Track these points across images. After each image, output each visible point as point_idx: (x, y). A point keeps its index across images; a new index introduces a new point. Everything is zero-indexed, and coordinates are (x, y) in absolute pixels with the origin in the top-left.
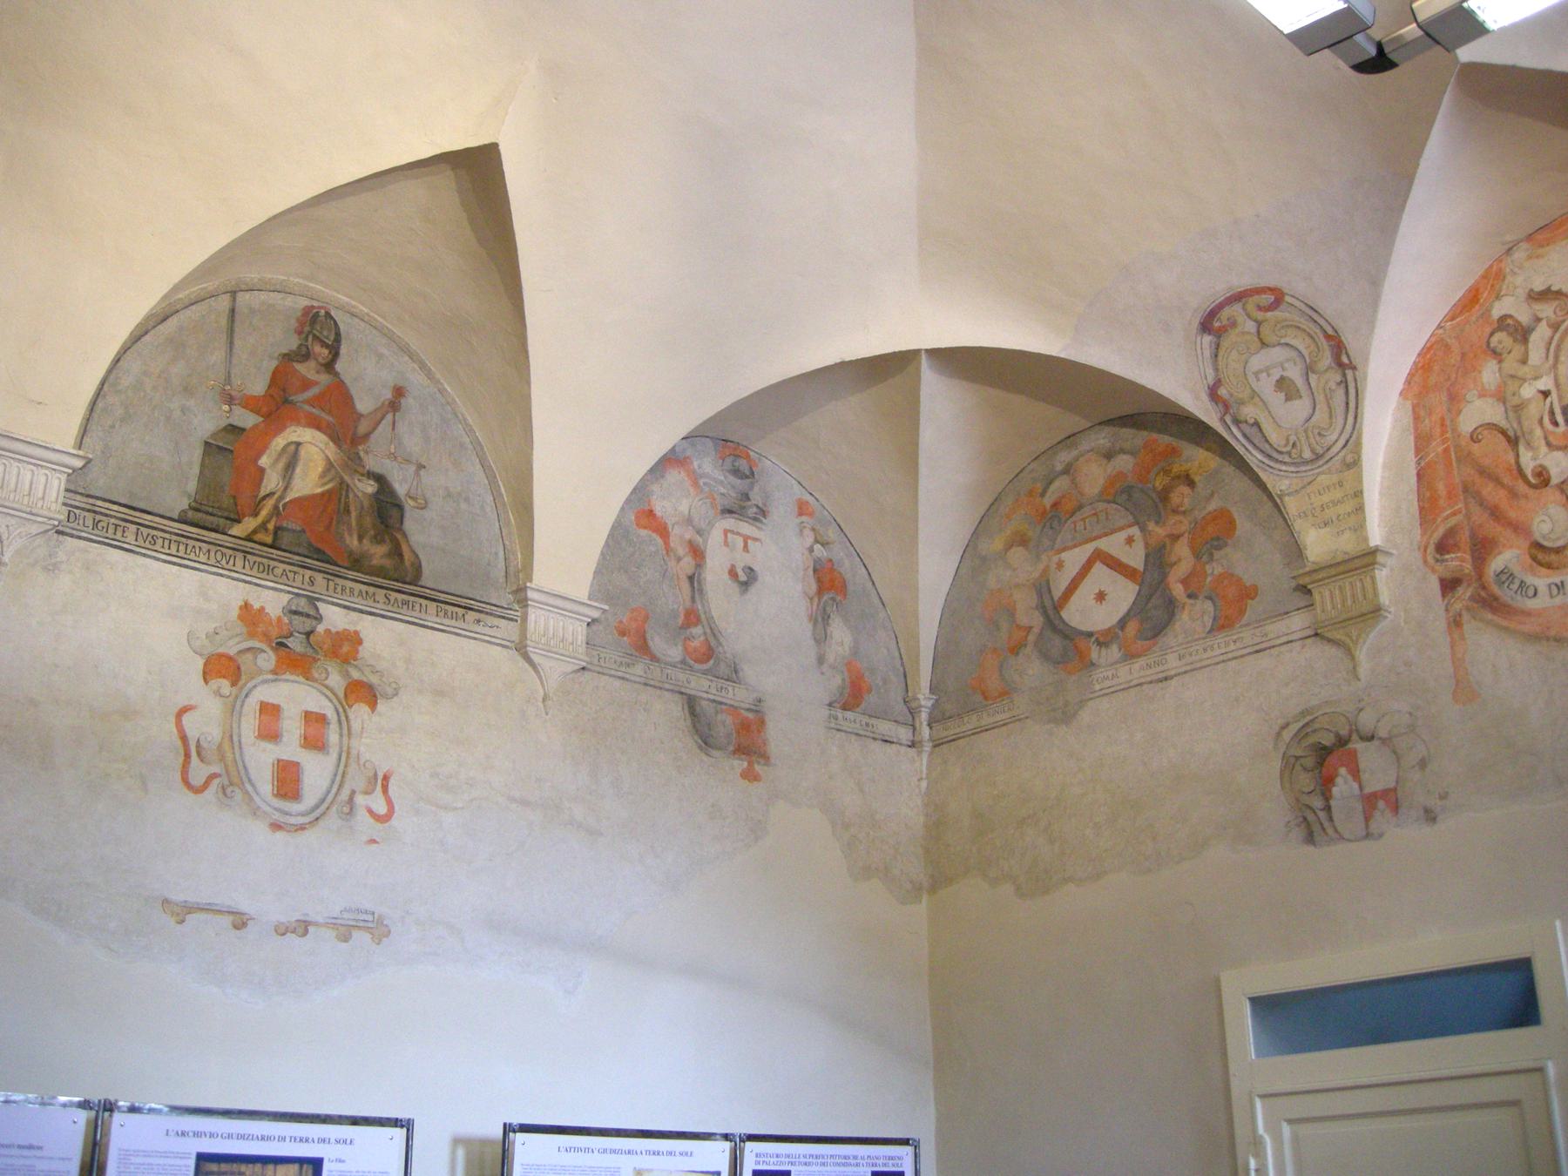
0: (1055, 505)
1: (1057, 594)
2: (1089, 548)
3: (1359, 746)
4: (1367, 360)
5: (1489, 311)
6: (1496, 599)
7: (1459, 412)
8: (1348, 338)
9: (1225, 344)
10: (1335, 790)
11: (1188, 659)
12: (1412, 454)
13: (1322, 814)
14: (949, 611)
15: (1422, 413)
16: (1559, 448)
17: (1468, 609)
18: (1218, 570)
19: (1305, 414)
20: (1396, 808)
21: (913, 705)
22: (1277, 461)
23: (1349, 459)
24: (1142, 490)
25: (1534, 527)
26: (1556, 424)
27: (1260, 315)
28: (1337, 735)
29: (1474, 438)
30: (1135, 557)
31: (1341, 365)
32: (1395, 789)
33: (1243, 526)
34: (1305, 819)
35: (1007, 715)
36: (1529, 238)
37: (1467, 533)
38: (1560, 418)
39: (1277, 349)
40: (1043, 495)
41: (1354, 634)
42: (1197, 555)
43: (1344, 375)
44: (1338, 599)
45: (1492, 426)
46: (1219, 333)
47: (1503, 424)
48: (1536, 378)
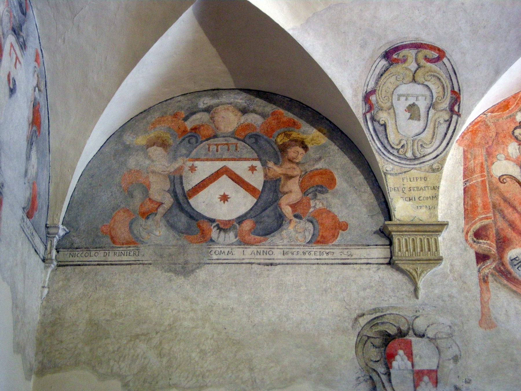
0: (194, 129)
1: (188, 187)
2: (219, 165)
3: (414, 339)
6: (510, 273)
7: (493, 163)
8: (464, 98)
9: (392, 70)
10: (395, 364)
11: (290, 255)
12: (461, 177)
13: (384, 378)
14: (374, 155)
15: (469, 156)
17: (492, 275)
18: (319, 206)
19: (417, 131)
20: (436, 383)
21: (51, 231)
22: (389, 152)
23: (435, 166)
24: (266, 140)
27: (423, 62)
28: (399, 329)
29: (501, 179)
30: (257, 180)
31: (452, 110)
32: (436, 371)
33: (341, 184)
34: (371, 377)
35: (133, 258)
37: (494, 231)
40: (186, 119)
42: (305, 191)
43: (451, 117)
44: (411, 246)
45: (512, 177)
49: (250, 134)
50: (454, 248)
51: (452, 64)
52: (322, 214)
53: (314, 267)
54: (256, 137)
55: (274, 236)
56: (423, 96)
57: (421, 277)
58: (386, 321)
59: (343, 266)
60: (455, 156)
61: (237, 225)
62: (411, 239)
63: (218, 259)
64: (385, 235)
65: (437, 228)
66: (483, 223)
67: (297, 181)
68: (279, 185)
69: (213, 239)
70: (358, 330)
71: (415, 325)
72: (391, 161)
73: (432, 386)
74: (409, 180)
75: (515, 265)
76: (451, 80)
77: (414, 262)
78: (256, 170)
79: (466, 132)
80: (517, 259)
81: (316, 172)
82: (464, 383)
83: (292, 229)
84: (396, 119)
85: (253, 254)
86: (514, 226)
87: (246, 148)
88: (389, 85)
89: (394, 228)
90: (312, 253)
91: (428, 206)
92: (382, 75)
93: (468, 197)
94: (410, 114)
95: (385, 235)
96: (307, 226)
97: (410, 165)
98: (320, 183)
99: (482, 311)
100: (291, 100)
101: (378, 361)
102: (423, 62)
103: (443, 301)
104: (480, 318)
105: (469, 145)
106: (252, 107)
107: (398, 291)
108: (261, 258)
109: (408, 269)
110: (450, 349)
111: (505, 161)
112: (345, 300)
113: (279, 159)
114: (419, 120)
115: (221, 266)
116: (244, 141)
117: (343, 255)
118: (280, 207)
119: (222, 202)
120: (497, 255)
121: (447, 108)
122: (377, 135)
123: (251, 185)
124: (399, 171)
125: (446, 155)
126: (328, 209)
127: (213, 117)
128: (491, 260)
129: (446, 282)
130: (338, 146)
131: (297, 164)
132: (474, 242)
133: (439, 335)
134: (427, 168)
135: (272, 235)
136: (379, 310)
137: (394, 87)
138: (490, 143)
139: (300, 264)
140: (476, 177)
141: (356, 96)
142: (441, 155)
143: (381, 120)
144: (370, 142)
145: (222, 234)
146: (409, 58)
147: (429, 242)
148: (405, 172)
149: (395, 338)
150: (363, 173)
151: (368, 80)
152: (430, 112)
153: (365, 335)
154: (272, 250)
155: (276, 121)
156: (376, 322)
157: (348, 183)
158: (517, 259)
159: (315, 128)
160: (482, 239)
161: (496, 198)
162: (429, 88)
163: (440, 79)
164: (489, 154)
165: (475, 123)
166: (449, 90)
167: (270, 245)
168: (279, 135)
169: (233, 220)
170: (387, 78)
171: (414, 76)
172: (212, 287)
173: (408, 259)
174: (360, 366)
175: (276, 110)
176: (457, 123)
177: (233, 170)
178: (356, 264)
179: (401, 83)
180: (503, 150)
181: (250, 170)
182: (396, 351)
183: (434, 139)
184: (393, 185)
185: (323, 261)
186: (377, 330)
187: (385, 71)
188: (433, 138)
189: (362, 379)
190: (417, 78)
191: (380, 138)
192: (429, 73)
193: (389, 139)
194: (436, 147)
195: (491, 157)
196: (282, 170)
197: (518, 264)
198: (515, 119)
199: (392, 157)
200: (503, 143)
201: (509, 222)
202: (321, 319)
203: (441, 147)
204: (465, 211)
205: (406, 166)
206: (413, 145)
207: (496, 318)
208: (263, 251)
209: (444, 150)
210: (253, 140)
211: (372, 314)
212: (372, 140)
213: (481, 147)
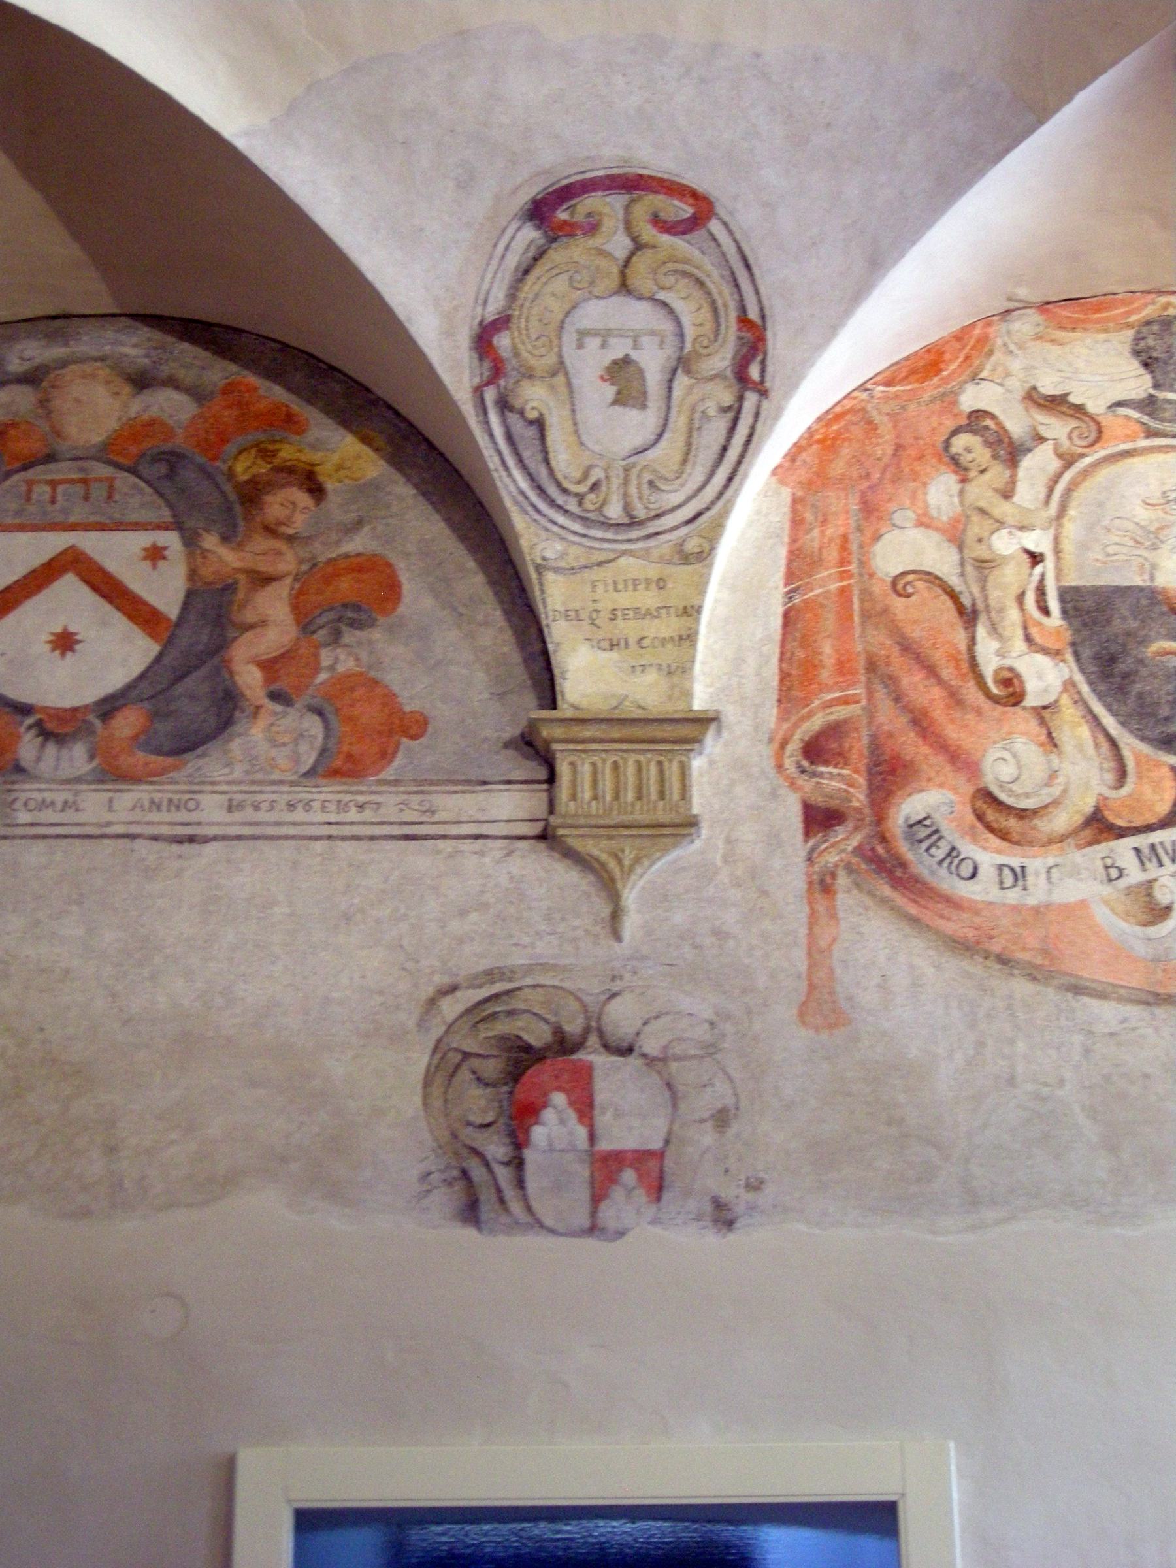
2: (54, 543)
4: (793, 386)
5: (955, 394)
6: (903, 865)
7: (877, 537)
8: (778, 340)
9: (557, 255)
10: (539, 1133)
11: (249, 814)
13: (503, 1174)
15: (809, 516)
16: (1045, 651)
17: (849, 868)
18: (346, 664)
19: (638, 441)
20: (658, 1189)
22: (552, 503)
23: (691, 546)
24: (203, 470)
26: (1046, 611)
27: (648, 233)
28: (558, 1032)
29: (899, 585)
30: (165, 590)
31: (742, 377)
32: (660, 1155)
33: (415, 598)
34: (465, 1174)
36: (1045, 307)
37: (865, 741)
38: (1054, 605)
39: (644, 307)
41: (628, 857)
42: (305, 622)
43: (741, 398)
44: (607, 784)
47: (954, 581)
48: (1022, 528)
49: (155, 451)
50: (739, 790)
51: (738, 236)
52: (352, 689)
53: (319, 846)
54: (174, 459)
55: (204, 755)
56: (653, 333)
57: (633, 877)
58: (522, 1006)
59: (402, 843)
60: (767, 515)
61: (98, 723)
62: (609, 763)
63: (32, 825)
64: (534, 749)
65: (684, 731)
66: (832, 718)
67: (285, 592)
68: (231, 603)
69: (23, 764)
70: (437, 1031)
71: (605, 1020)
74: (611, 588)
75: (920, 841)
76: (737, 286)
77: (613, 832)
78: (164, 558)
79: (804, 442)
80: (927, 822)
81: (342, 564)
82: (742, 1191)
83: (260, 736)
84: (573, 404)
85: (138, 810)
86: (925, 724)
87: (141, 492)
88: (550, 301)
89: (558, 732)
90: (316, 805)
91: (665, 666)
92: (526, 272)
93: (795, 640)
94: (614, 389)
95: (537, 752)
96: (306, 724)
98: (355, 596)
99: (810, 979)
100: (285, 347)
101: (489, 1125)
102: (648, 233)
103: (696, 947)
105: (810, 483)
106: (165, 370)
107: (563, 919)
108: (163, 821)
109: (596, 852)
110: (709, 1089)
111: (915, 531)
112: (405, 942)
113: (235, 526)
114: (644, 406)
115: (41, 845)
116: (133, 471)
117: (407, 811)
118: (228, 667)
119: (57, 653)
120: (867, 811)
121: (729, 373)
123: (145, 604)
124: (583, 562)
125: (725, 513)
126: (373, 674)
127: (48, 400)
128: (850, 825)
129: (711, 891)
130: (416, 486)
131: (290, 539)
132: (803, 772)
133: (678, 1049)
134: (666, 550)
135: (199, 751)
136: (503, 974)
137: (567, 307)
138: (876, 476)
139: (279, 838)
140: (822, 579)
141: (449, 334)
143: (528, 407)
144: (495, 475)
145: (51, 750)
146: (606, 219)
147: (661, 772)
148: (600, 564)
150: (483, 565)
151: (485, 286)
152: (676, 384)
153: (456, 1050)
154: (198, 797)
155: (235, 412)
156: (490, 1008)
157: (436, 597)
158: (927, 822)
159: (351, 431)
160: (826, 763)
164: (869, 509)
165: (831, 417)
166: (733, 315)
167: (191, 783)
168: (240, 452)
169: (86, 707)
170: (544, 279)
171: (623, 274)
172: (10, 908)
174: (436, 1139)
175: (239, 378)
176: (757, 415)
177: (97, 557)
178: (444, 837)
179: (587, 295)
180: (913, 497)
181: (145, 558)
182: (545, 1095)
184: (564, 603)
185: (347, 831)
186: (491, 1034)
187: (536, 259)
188: (684, 461)
189: (435, 1178)
190: (634, 282)
191: (526, 461)
192: (670, 266)
193: (553, 463)
194: (695, 487)
196: (242, 560)
197: (929, 836)
198: (955, 403)
199: (561, 519)
200: (915, 476)
201: (911, 711)
202: (327, 1000)
204: (782, 680)
206: (626, 482)
207: (850, 999)
208: (170, 801)
210: (163, 469)
211: (480, 986)
212: (501, 469)
213: (843, 489)
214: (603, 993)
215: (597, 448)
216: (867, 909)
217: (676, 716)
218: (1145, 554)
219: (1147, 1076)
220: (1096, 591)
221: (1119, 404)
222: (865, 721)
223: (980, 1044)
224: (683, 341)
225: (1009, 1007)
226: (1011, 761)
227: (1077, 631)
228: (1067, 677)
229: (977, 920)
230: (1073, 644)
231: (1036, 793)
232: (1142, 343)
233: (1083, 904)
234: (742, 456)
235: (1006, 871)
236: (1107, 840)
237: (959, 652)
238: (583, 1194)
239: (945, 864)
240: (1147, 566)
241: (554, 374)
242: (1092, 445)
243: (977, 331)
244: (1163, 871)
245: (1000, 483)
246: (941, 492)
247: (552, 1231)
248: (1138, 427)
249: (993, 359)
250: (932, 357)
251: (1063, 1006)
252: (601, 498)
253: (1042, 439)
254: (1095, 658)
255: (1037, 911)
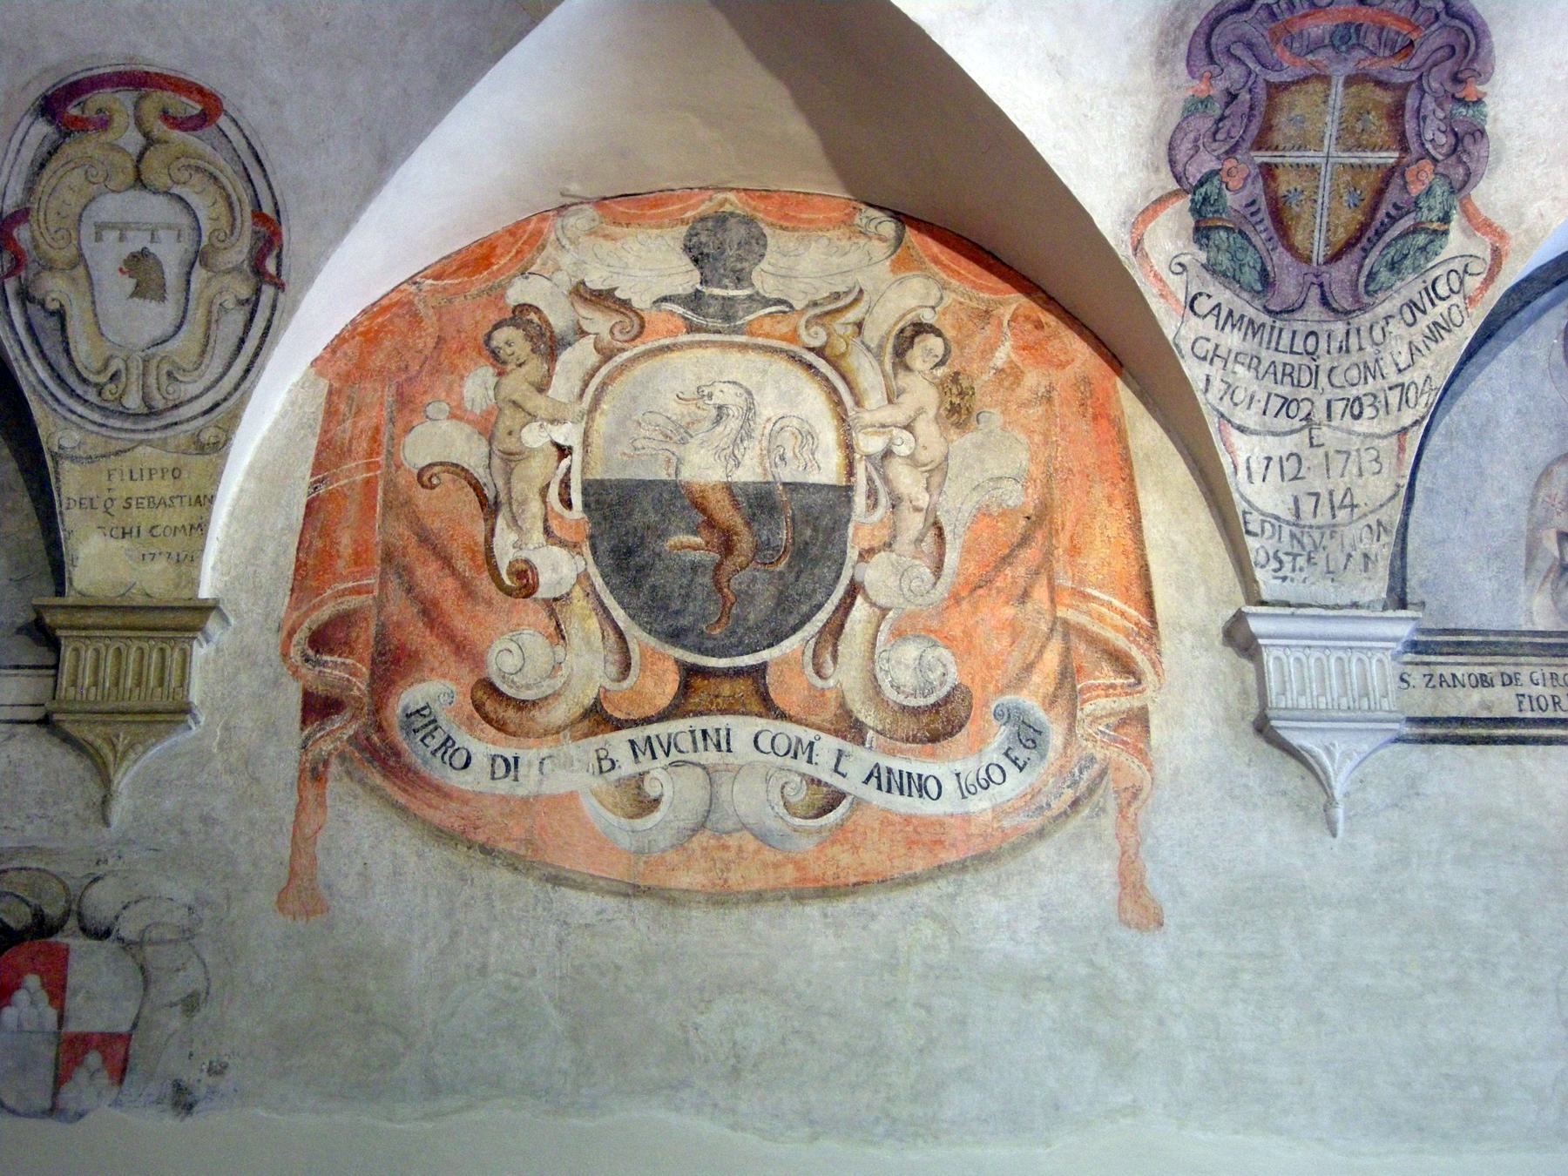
4: (309, 280)
7: (409, 429)
8: (293, 234)
9: (71, 149)
15: (343, 407)
16: (562, 544)
17: (342, 757)
19: (158, 333)
20: (121, 1072)
22: (72, 393)
23: (207, 436)
25: (491, 657)
26: (568, 504)
27: (159, 129)
28: (39, 916)
29: (424, 478)
31: (258, 270)
37: (373, 630)
38: (577, 498)
43: (258, 291)
45: (458, 470)
46: (68, 129)
47: (480, 473)
48: (553, 421)
50: (243, 678)
56: (169, 227)
57: (125, 764)
64: (42, 634)
65: (186, 618)
71: (87, 902)
72: (78, 420)
73: (106, 1081)
74: (127, 477)
75: (415, 731)
76: (250, 181)
80: (426, 712)
82: (205, 1074)
88: (70, 197)
89: (61, 618)
92: (42, 166)
97: (133, 431)
99: (292, 868)
102: (159, 129)
103: (183, 833)
104: (284, 884)
105: (348, 374)
107: (55, 803)
109: (90, 738)
110: (181, 973)
111: (447, 423)
114: (163, 299)
120: (366, 700)
122: (36, 342)
124: (100, 451)
128: (347, 714)
132: (307, 660)
133: (155, 934)
134: (183, 440)
137: (84, 201)
142: (226, 405)
143: (48, 299)
146: (117, 117)
147: (163, 659)
148: (117, 453)
149: (24, 940)
152: (193, 278)
158: (426, 712)
160: (331, 652)
161: (400, 532)
162: (187, 206)
163: (216, 179)
166: (248, 210)
173: (88, 708)
176: (274, 308)
180: (449, 391)
182: (20, 976)
183: (208, 356)
187: (50, 154)
188: (203, 352)
191: (47, 352)
193: (74, 354)
195: (406, 412)
198: (503, 296)
199: (80, 409)
200: (453, 368)
203: (226, 379)
204: (297, 570)
205: (123, 435)
209: (236, 388)
214: (87, 876)
215: (117, 339)
216: (356, 797)
217: (176, 604)
218: (674, 449)
219: (618, 968)
220: (619, 484)
221: (665, 299)
222: (374, 611)
223: (454, 934)
224: (200, 236)
225: (488, 896)
226: (517, 653)
227: (596, 524)
228: (581, 569)
229: (466, 809)
230: (591, 537)
231: (537, 685)
232: (695, 239)
233: (572, 796)
234: (260, 347)
235: (499, 761)
236: (603, 732)
237: (476, 544)
238: (46, 1074)
239: (439, 754)
240: (674, 460)
241: (73, 266)
242: (633, 339)
243: (532, 226)
244: (656, 763)
245: (536, 378)
246: (477, 386)
247: (13, 1112)
248: (680, 322)
249: (544, 254)
250: (484, 250)
251: (541, 896)
252: (121, 387)
253: (583, 333)
254: (612, 551)
255: (525, 801)
